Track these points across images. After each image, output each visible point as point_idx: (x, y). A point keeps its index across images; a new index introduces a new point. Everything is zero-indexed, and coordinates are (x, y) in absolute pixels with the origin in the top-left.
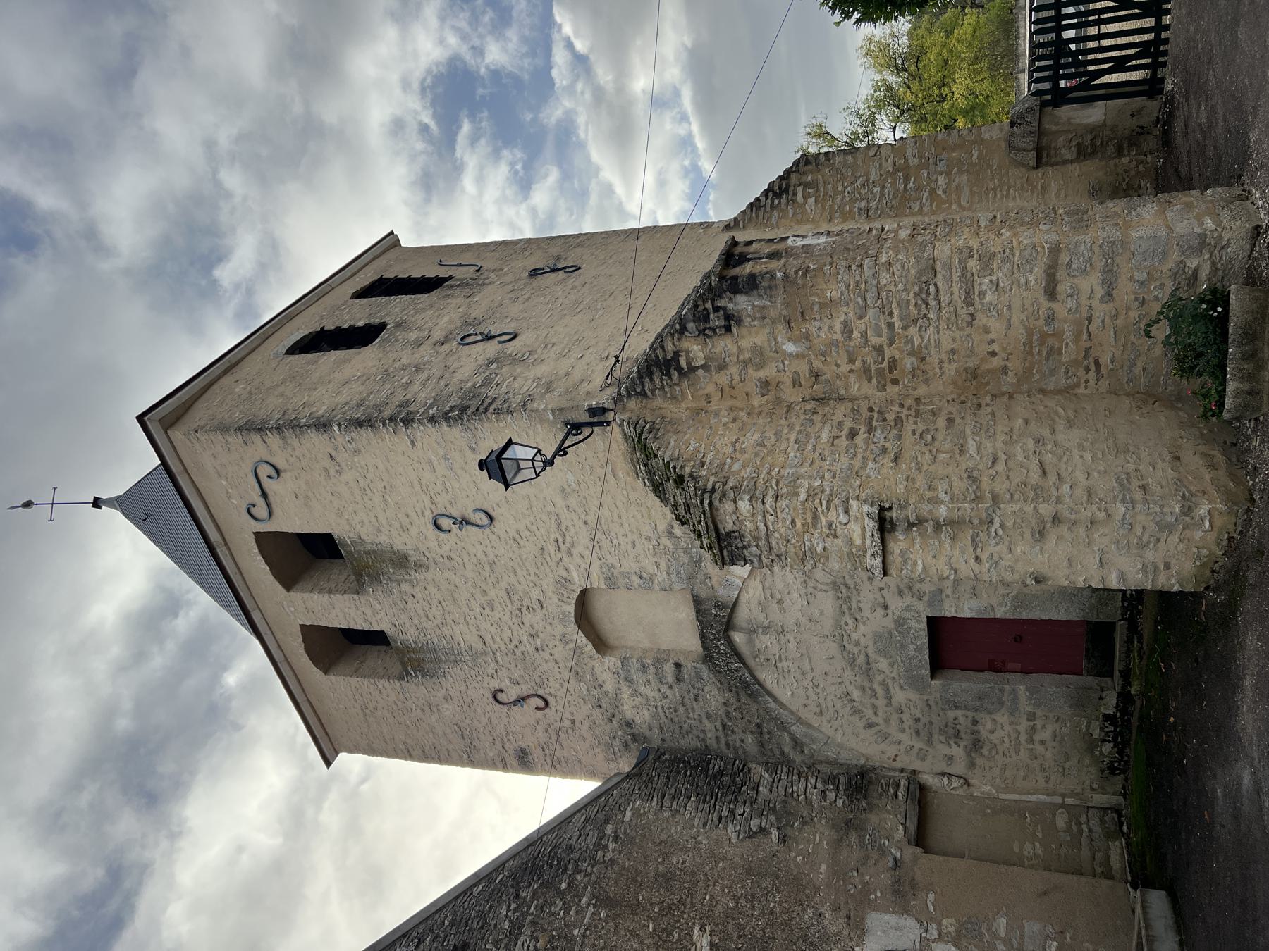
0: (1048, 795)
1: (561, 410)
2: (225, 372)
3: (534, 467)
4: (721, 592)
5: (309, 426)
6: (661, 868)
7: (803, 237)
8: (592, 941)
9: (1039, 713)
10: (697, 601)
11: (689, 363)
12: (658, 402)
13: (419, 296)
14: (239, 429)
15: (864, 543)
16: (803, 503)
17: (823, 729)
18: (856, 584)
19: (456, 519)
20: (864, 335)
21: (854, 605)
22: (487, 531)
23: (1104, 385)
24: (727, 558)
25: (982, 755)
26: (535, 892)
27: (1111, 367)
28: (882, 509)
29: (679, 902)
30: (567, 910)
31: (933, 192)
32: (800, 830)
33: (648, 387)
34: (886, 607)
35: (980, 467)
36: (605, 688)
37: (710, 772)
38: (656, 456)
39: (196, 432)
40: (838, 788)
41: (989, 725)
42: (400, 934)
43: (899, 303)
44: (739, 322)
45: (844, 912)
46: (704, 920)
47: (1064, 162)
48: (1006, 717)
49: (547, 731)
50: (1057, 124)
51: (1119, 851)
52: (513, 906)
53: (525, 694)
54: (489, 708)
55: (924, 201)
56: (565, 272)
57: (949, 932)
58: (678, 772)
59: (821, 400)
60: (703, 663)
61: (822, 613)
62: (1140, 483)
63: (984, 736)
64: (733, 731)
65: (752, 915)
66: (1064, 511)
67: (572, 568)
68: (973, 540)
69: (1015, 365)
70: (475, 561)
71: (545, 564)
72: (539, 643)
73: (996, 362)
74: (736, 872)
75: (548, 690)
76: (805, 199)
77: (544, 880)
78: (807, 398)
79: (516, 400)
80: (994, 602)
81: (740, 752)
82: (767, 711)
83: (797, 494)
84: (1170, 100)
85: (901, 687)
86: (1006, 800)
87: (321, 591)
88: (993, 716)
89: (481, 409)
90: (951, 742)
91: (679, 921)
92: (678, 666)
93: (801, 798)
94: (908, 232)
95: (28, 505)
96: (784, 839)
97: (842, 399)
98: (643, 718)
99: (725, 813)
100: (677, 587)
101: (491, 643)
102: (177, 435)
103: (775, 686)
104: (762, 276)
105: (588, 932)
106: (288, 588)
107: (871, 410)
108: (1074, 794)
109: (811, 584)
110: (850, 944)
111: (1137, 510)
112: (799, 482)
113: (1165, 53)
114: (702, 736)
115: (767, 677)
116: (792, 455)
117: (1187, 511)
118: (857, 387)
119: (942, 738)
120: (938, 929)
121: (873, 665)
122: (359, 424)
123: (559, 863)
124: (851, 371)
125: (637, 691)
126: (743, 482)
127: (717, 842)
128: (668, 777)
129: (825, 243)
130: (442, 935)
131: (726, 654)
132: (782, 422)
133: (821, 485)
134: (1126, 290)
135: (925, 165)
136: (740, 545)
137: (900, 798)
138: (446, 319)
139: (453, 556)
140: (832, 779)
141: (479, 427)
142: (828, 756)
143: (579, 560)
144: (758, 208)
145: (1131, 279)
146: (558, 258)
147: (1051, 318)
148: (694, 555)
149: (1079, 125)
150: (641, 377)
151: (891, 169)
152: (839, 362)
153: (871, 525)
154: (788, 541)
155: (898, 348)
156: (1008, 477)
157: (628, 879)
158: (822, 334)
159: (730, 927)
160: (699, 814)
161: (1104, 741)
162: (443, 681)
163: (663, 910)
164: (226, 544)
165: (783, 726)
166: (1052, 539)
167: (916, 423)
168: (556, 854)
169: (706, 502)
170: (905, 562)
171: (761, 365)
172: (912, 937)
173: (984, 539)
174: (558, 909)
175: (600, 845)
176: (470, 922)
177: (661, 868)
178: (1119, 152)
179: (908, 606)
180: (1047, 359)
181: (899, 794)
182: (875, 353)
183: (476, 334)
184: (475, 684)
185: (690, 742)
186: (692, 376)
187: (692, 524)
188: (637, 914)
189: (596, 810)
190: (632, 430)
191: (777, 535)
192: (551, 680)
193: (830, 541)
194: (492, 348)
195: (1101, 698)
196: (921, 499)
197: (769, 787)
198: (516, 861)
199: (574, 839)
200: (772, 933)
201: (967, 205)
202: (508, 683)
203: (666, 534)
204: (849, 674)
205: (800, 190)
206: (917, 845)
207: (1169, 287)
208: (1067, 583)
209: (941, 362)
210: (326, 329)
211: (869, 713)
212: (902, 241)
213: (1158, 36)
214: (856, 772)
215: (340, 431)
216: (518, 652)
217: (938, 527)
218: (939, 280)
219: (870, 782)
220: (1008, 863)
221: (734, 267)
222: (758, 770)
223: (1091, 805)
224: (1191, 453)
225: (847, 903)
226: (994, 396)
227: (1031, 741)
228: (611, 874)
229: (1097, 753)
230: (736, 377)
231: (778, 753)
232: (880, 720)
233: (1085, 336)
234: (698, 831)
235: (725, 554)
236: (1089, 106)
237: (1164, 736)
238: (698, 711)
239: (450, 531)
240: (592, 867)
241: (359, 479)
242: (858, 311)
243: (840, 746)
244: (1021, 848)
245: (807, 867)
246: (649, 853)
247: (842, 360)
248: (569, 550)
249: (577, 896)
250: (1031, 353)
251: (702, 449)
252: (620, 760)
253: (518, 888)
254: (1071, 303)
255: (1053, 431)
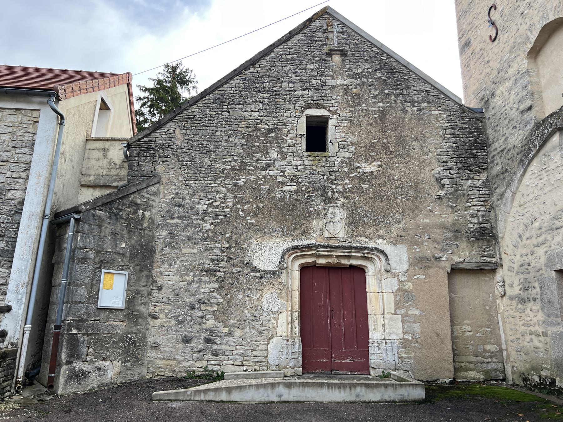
0: (505, 341)
6: (409, 138)
8: (361, 114)
9: (548, 339)
17: (513, 209)
25: (517, 304)
26: (380, 78)
29: (391, 151)
30: (374, 97)
37: (475, 151)
40: (481, 223)
41: (535, 308)
42: (344, 22)
45: (403, 234)
46: (384, 166)
48: (542, 318)
51: (477, 377)
57: (404, 286)
60: (535, 123)
63: (528, 305)
64: (501, 157)
65: (392, 189)
72: (526, 12)
74: (414, 176)
77: (388, 80)
82: (515, 173)
85: (546, 252)
86: (497, 318)
88: (540, 311)
90: (521, 286)
91: (381, 153)
93: (469, 204)
96: (440, 198)
99: (449, 164)
105: (365, 111)
108: (509, 356)
110: (387, 238)
114: (495, 140)
119: (522, 280)
120: (405, 280)
121: (556, 232)
123: (399, 85)
125: (511, 90)
128: (466, 128)
130: (348, 42)
131: (543, 135)
137: (482, 258)
140: (486, 219)
142: (499, 215)
157: (398, 123)
159: (383, 179)
160: (446, 150)
161: (540, 377)
163: (385, 145)
165: (509, 185)
168: (404, 82)
172: (398, 268)
174: (373, 93)
176: (357, 52)
177: (409, 138)
181: (485, 258)
185: (490, 133)
188: (380, 132)
189: (435, 94)
197: (472, 185)
198: (395, 63)
200: (384, 200)
204: (547, 218)
211: (527, 235)
214: (494, 232)
219: (488, 241)
222: (483, 177)
223: (505, 365)
225: (409, 234)
227: (531, 334)
228: (399, 113)
229: (532, 372)
231: (495, 186)
232: (524, 242)
234: (434, 152)
237: (520, 415)
238: (507, 132)
240: (400, 103)
243: (506, 221)
244: (468, 325)
245: (425, 212)
246: (415, 129)
249: (383, 100)
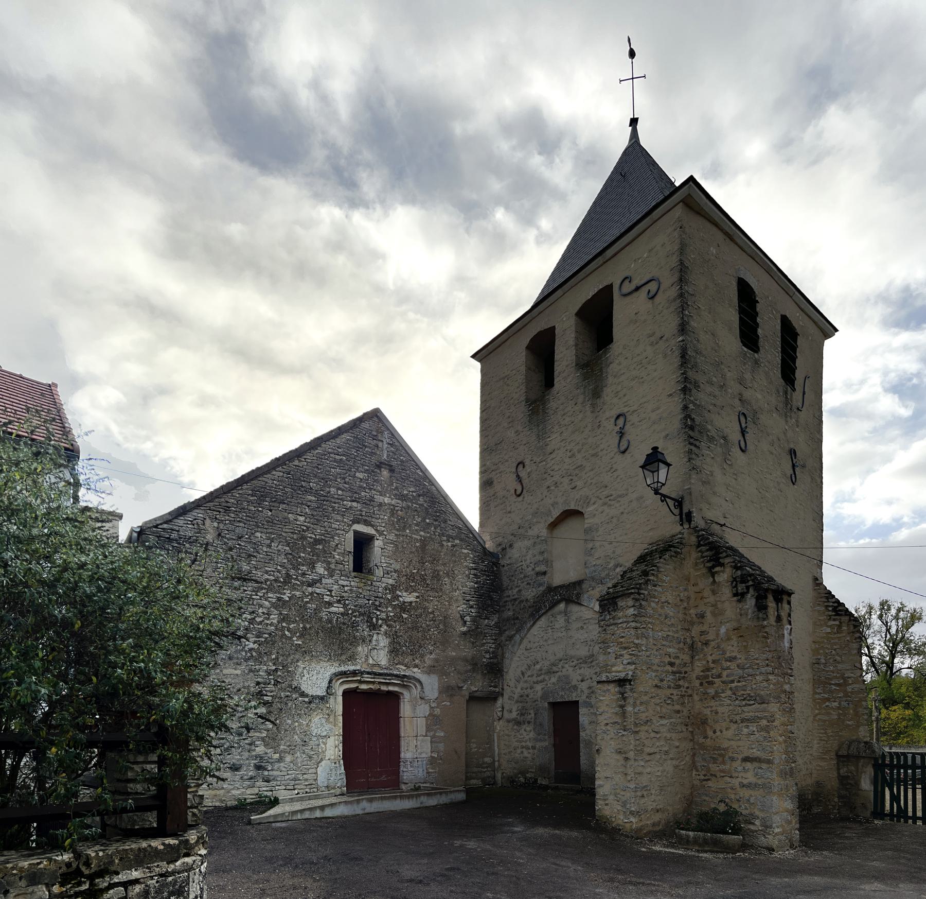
0: (498, 754)
1: (690, 494)
2: (726, 234)
3: (654, 483)
4: (586, 596)
5: (682, 318)
6: (441, 573)
7: (790, 634)
9: (536, 751)
10: (579, 583)
11: (716, 572)
12: (694, 555)
13: (780, 371)
14: (681, 263)
15: (613, 672)
16: (633, 642)
18: (593, 666)
19: (623, 429)
20: (728, 668)
21: (583, 665)
22: (616, 450)
23: (697, 783)
24: (603, 603)
26: (422, 505)
27: (706, 786)
28: (630, 681)
31: (828, 700)
32: (470, 641)
33: (704, 548)
34: (582, 681)
35: (653, 726)
36: (529, 530)
37: (492, 594)
38: (660, 558)
39: (681, 228)
41: (528, 729)
42: (393, 432)
43: (745, 685)
44: (739, 601)
45: (436, 664)
47: (838, 769)
49: (504, 497)
50: (863, 766)
52: (414, 494)
53: (523, 482)
54: (514, 460)
55: (822, 695)
56: (791, 475)
58: (488, 576)
59: (692, 647)
61: (578, 649)
62: (645, 795)
64: (513, 605)
66: (631, 762)
67: (595, 506)
68: (616, 722)
69: (708, 742)
70: (598, 443)
71: (598, 488)
72: (552, 488)
73: (710, 733)
75: (526, 496)
76: (830, 626)
78: (694, 639)
79: (697, 462)
80: (587, 732)
81: (502, 609)
82: (525, 623)
83: (638, 638)
84: (867, 821)
87: (576, 338)
89: (692, 440)
92: (545, 573)
94: (788, 690)
95: (632, 54)
97: (692, 657)
98: (514, 553)
100: (587, 571)
101: (551, 458)
102: (679, 211)
103: (539, 626)
104: (765, 613)
105: (408, 538)
106: (577, 314)
107: (686, 673)
108: (500, 766)
109: (592, 643)
111: (632, 793)
112: (644, 639)
113: (899, 821)
115: (542, 622)
116: (660, 634)
117: (632, 813)
118: (699, 666)
119: (520, 708)
121: (553, 675)
122: (684, 355)
123: (438, 516)
124: (708, 662)
126: (645, 610)
127: (457, 600)
129: (785, 647)
132: (680, 627)
133: (643, 650)
134: (745, 793)
135: (846, 695)
136: (610, 610)
138: (759, 397)
139: (601, 428)
141: (680, 440)
143: (600, 510)
144: (827, 598)
145: (751, 796)
146: (803, 466)
147: (732, 759)
148: (605, 580)
149: (861, 778)
150: (710, 543)
151: (846, 675)
152: (713, 655)
153: (622, 675)
154: (613, 635)
155: (720, 686)
156: (648, 738)
158: (730, 647)
159: (420, 611)
161: (525, 778)
162: (527, 429)
164: (605, 263)
165: (518, 631)
166: (618, 757)
167: (677, 695)
168: (442, 514)
169: (633, 591)
170: (604, 691)
171: (714, 615)
173: (616, 728)
175: (449, 537)
178: (840, 797)
179: (583, 691)
180: (711, 757)
182: (717, 674)
183: (746, 423)
184: (526, 450)
185: (505, 581)
186: (709, 574)
187: (621, 581)
190: (677, 541)
191: (616, 629)
192: (532, 498)
193: (614, 656)
194: (735, 436)
195: (545, 778)
196: (636, 699)
199: (450, 523)
201: (817, 719)
202: (528, 471)
203: (616, 563)
204: (547, 663)
205: (837, 623)
206: (469, 697)
207: (744, 812)
208: (597, 763)
209: (711, 707)
210: (757, 304)
211: (529, 673)
212: (782, 686)
213: (910, 818)
215: (679, 342)
216: (546, 476)
217: (622, 707)
218: (757, 706)
220: (467, 737)
221: (773, 596)
224: (661, 817)
225: (440, 666)
226: (692, 732)
227: (523, 747)
230: (708, 600)
231: (505, 628)
232: (526, 678)
233: (722, 775)
235: (605, 602)
236: (871, 782)
239: (616, 425)
241: (647, 359)
242: (742, 665)
243: (512, 659)
244: (473, 743)
247: (714, 657)
248: (606, 504)
250: (714, 750)
251: (664, 584)
252: (491, 542)
253: (423, 495)
254: (740, 769)
255: (672, 759)
